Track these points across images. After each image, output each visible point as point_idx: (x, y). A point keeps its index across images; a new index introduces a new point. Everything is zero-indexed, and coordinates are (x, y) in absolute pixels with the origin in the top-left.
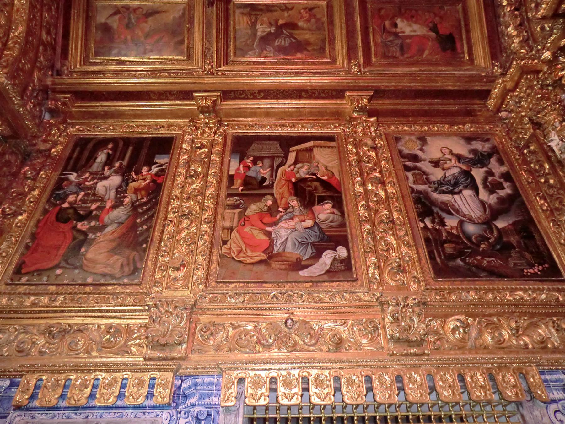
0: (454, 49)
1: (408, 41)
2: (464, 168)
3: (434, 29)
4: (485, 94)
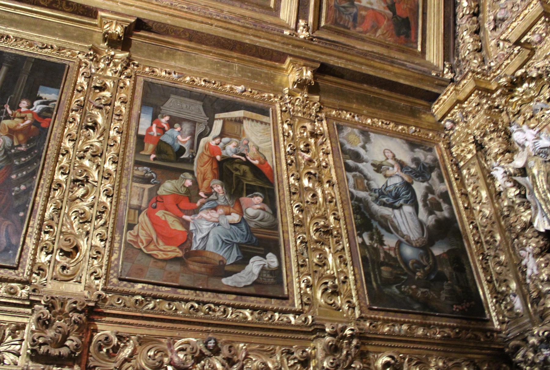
0: (408, 36)
1: (364, 13)
2: (406, 179)
3: (392, 7)
4: (433, 97)
